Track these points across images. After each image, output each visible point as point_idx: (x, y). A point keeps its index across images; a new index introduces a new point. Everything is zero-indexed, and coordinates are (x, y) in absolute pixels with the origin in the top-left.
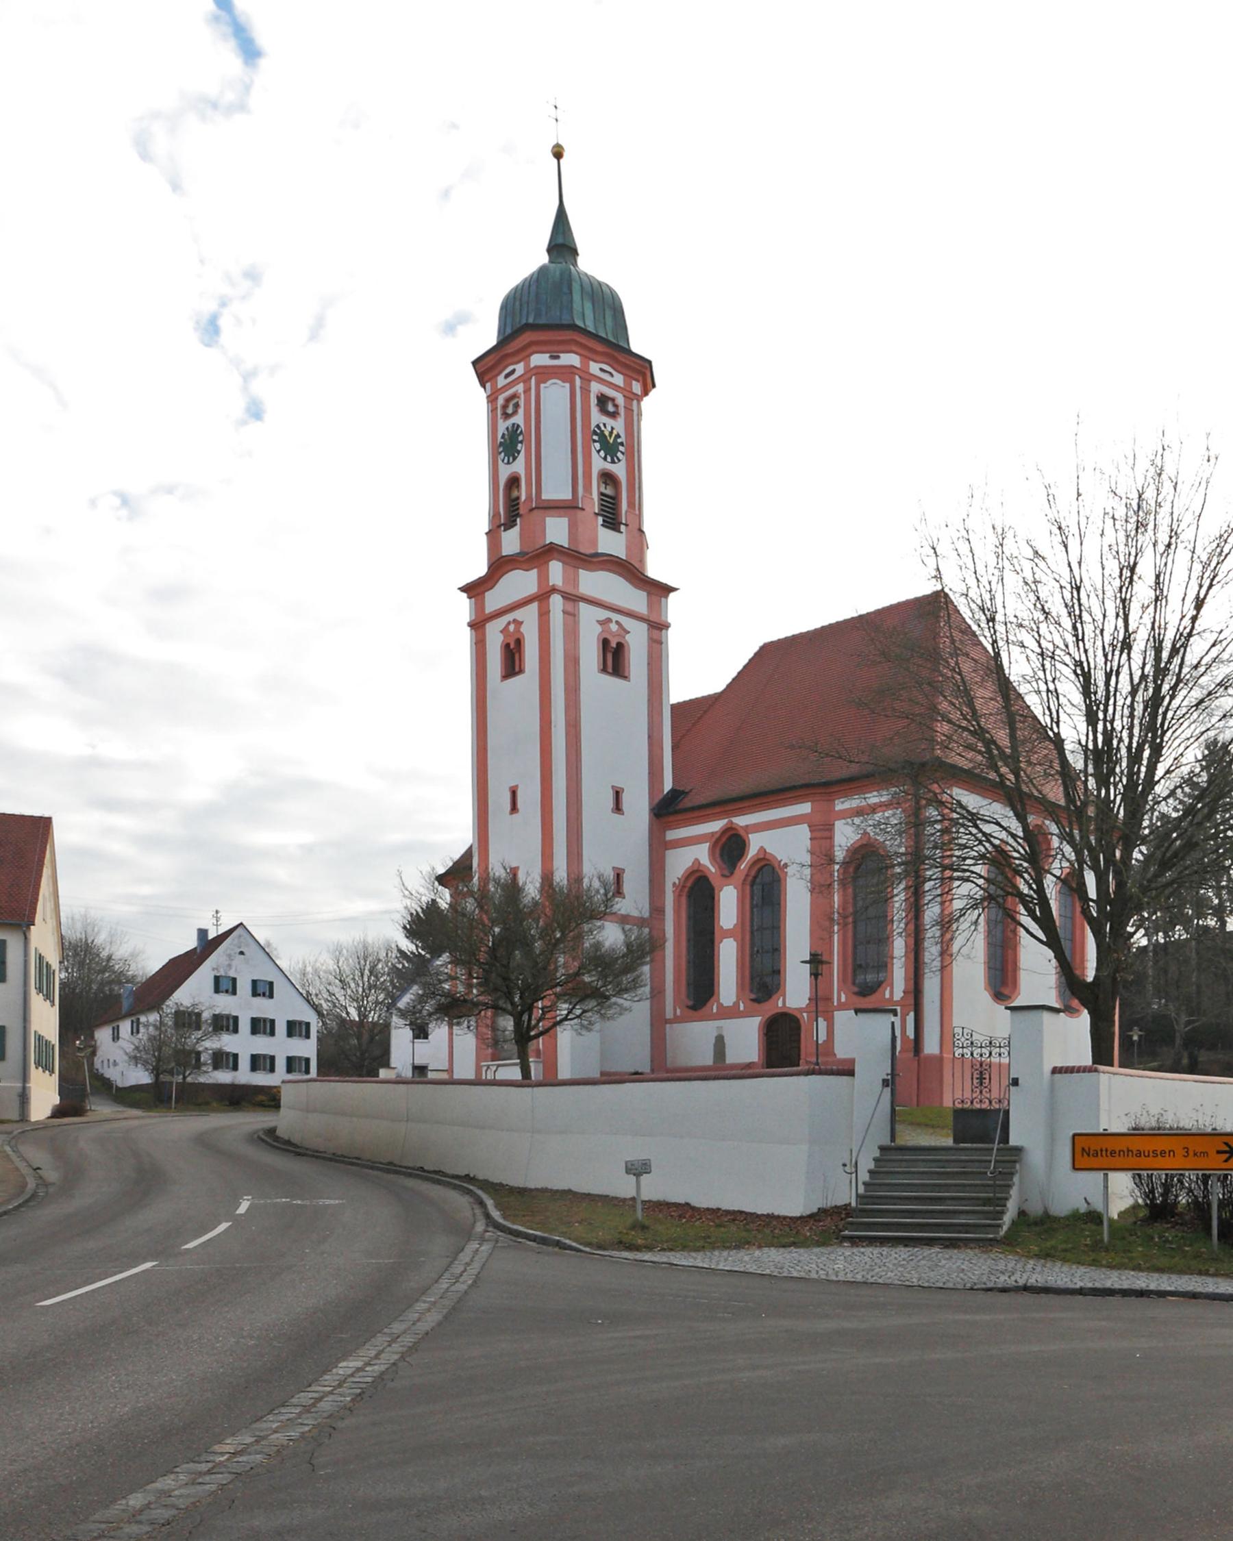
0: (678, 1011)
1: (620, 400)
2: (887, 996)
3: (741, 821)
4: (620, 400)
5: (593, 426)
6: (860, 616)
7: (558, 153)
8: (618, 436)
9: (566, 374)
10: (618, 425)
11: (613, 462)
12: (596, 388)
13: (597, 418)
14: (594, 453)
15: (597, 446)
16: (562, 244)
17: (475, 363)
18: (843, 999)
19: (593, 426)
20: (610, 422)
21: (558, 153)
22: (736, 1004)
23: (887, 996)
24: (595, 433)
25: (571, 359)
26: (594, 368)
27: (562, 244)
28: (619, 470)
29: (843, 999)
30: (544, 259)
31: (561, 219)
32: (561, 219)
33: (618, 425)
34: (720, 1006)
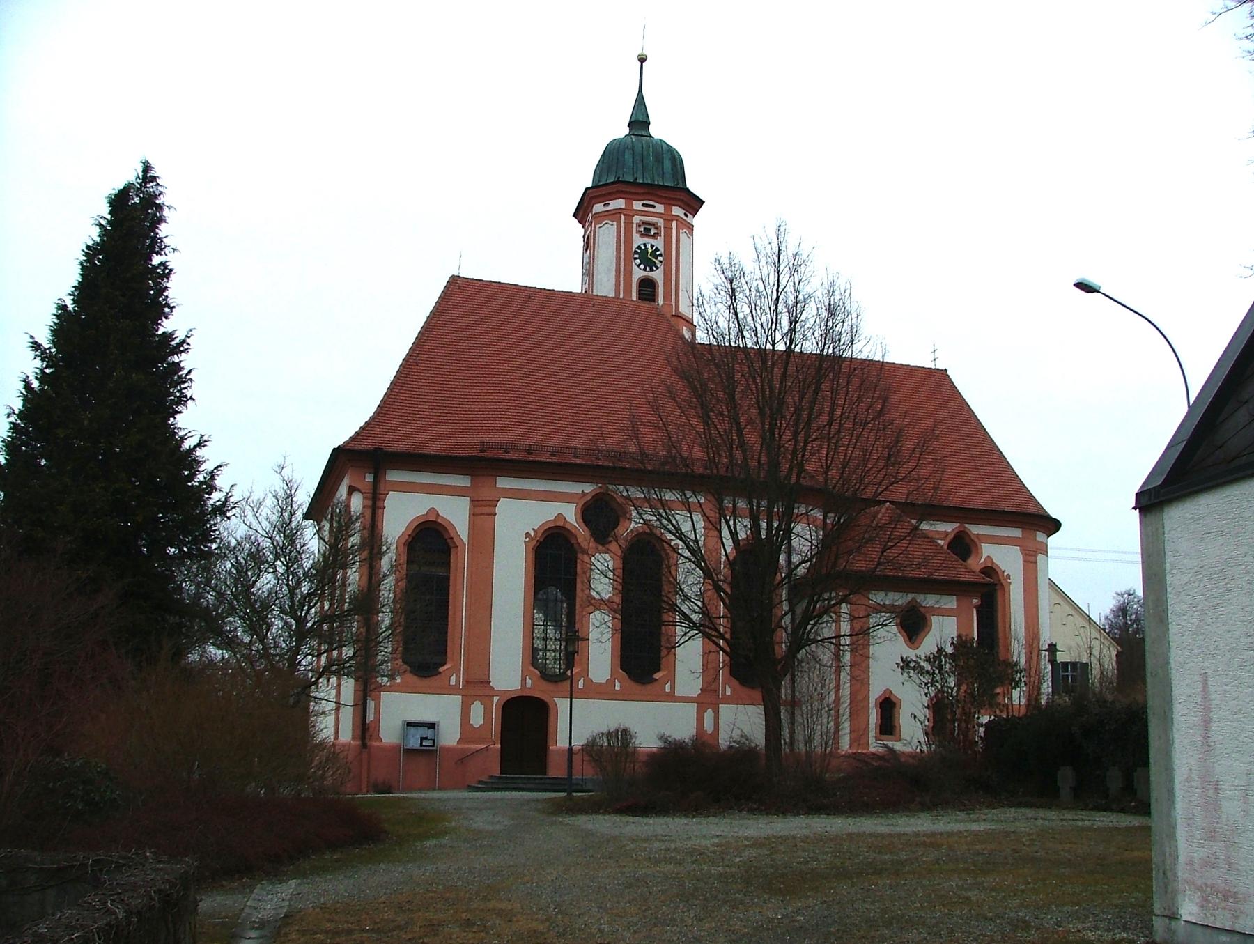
0: (528, 681)
1: (660, 222)
2: (668, 689)
3: (975, 529)
4: (660, 222)
5: (634, 248)
6: (883, 364)
7: (642, 60)
8: (657, 249)
9: (613, 215)
10: (659, 243)
11: (652, 270)
12: (636, 219)
13: (638, 241)
14: (635, 267)
15: (638, 261)
16: (639, 122)
17: (574, 216)
18: (728, 692)
19: (634, 248)
20: (652, 241)
21: (642, 60)
22: (611, 682)
23: (668, 689)
24: (636, 252)
25: (619, 203)
26: (637, 205)
27: (639, 122)
28: (658, 275)
29: (728, 692)
30: (627, 131)
31: (640, 101)
32: (640, 101)
33: (659, 243)
34: (588, 682)
